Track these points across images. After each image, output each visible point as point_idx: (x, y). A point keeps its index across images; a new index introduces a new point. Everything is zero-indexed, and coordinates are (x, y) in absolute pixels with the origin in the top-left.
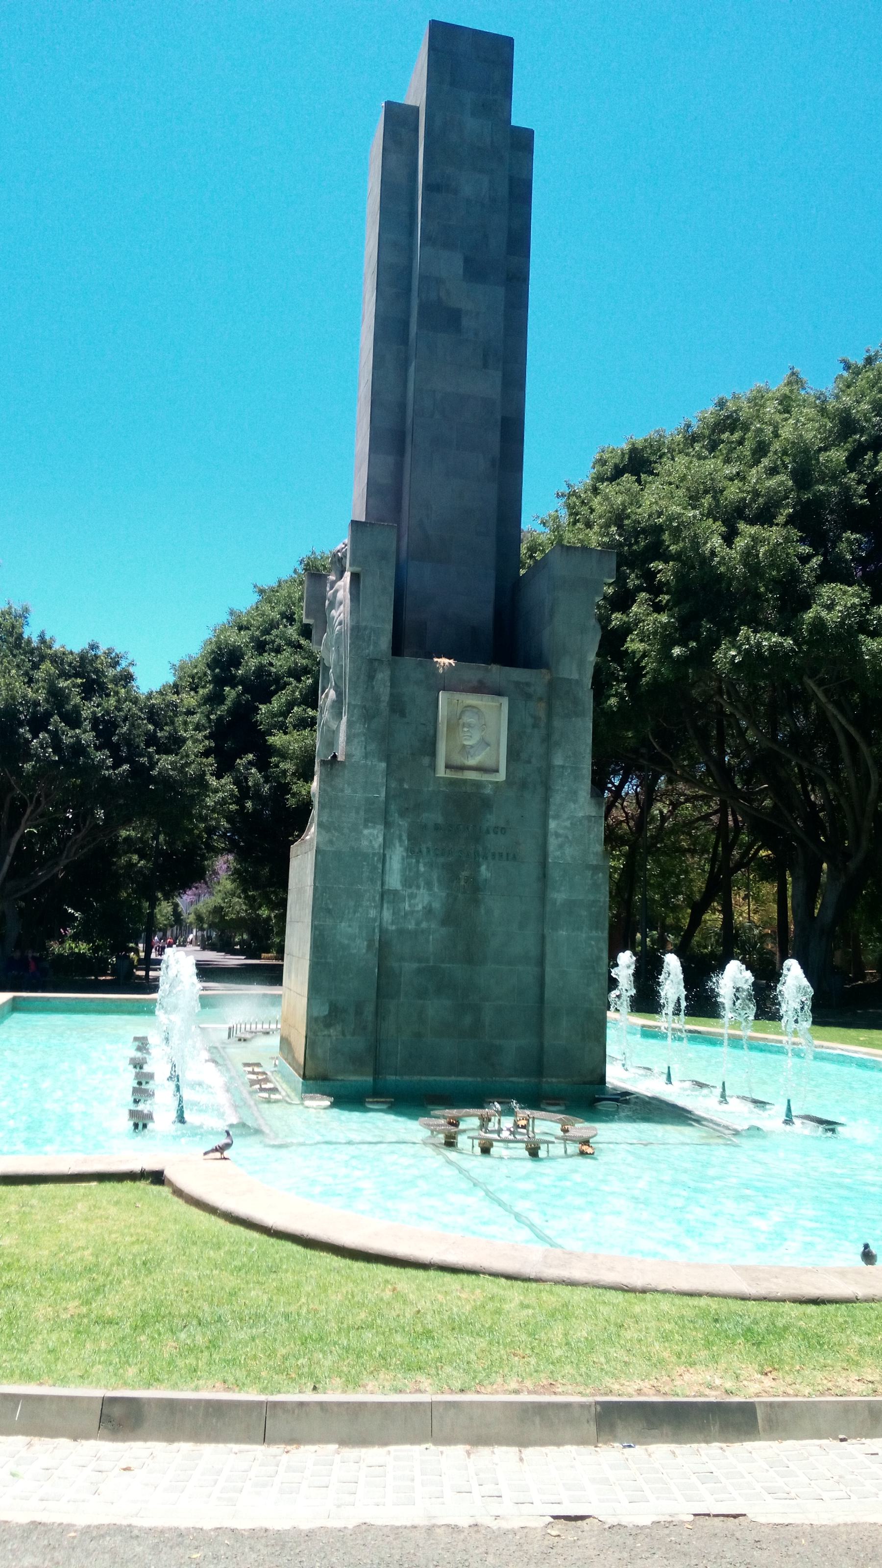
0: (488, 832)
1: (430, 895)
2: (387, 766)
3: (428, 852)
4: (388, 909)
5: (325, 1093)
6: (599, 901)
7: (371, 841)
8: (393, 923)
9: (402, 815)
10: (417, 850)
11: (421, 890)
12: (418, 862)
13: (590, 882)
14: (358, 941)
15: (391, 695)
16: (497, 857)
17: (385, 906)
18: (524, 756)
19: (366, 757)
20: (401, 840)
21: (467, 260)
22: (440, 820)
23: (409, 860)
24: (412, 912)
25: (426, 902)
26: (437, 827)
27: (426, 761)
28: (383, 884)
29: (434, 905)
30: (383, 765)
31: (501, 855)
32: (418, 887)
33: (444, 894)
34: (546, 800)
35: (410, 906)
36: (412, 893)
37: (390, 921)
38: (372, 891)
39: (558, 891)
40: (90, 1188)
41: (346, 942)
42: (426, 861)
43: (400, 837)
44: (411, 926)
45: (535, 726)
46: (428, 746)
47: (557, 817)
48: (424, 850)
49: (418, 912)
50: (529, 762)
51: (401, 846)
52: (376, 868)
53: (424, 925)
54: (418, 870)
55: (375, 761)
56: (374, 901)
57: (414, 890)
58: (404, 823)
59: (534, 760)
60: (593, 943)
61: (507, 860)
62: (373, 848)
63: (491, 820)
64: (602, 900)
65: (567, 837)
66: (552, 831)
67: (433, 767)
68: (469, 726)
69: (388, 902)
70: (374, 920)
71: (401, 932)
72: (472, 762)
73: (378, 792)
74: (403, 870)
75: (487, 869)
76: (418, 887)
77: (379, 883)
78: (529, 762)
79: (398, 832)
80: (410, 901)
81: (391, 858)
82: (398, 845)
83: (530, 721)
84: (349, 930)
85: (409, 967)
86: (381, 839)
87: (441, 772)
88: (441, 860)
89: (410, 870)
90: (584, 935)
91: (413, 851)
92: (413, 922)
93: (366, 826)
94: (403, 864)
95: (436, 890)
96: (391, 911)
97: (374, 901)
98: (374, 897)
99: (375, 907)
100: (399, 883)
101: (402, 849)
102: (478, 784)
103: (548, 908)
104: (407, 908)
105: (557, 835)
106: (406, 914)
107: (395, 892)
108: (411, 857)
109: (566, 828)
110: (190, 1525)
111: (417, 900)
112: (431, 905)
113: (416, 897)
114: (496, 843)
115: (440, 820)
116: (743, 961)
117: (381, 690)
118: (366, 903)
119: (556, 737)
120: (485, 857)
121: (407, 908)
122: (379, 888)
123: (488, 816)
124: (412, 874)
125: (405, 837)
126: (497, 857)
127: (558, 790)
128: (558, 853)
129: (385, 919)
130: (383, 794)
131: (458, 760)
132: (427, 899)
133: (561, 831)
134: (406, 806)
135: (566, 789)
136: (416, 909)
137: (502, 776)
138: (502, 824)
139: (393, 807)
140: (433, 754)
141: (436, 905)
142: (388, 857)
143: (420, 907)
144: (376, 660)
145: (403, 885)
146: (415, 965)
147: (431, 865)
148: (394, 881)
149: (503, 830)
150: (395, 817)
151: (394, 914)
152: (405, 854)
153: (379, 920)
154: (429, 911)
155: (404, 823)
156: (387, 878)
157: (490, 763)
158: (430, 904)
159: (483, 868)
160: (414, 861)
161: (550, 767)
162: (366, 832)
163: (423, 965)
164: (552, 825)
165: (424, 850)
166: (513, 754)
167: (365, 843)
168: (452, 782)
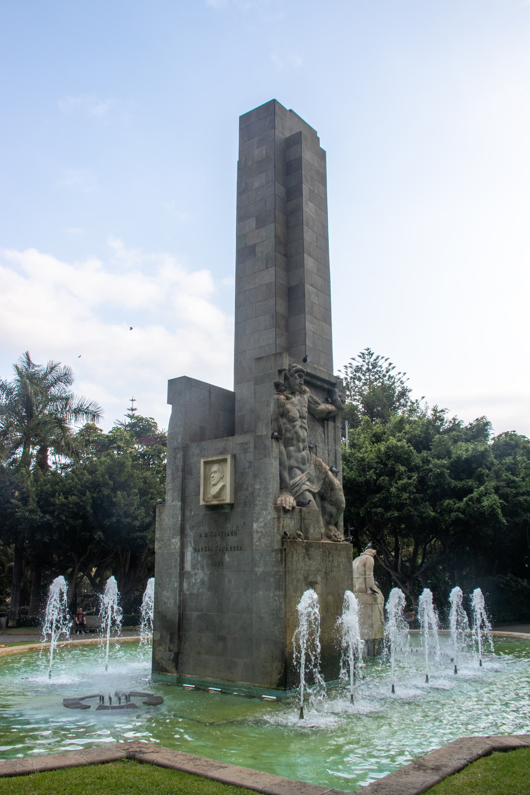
1: (203, 573)
3: (202, 549)
5: (49, 586)
6: (280, 571)
8: (188, 590)
12: (198, 555)
13: (274, 560)
14: (171, 600)
19: (173, 501)
20: (191, 544)
22: (207, 530)
24: (196, 583)
32: (198, 569)
33: (209, 572)
35: (195, 580)
39: (259, 567)
43: (191, 541)
44: (195, 592)
53: (201, 590)
56: (177, 578)
60: (277, 598)
62: (176, 549)
64: (281, 570)
65: (262, 533)
71: (191, 594)
74: (192, 559)
76: (198, 569)
78: (247, 489)
84: (167, 594)
85: (195, 614)
92: (196, 589)
93: (173, 538)
99: (177, 581)
104: (194, 581)
105: (257, 532)
106: (193, 584)
109: (261, 527)
115: (207, 530)
116: (320, 595)
121: (194, 581)
123: (228, 525)
125: (192, 542)
128: (258, 543)
132: (202, 575)
133: (259, 530)
135: (261, 503)
136: (197, 581)
138: (234, 529)
141: (206, 579)
145: (192, 568)
146: (197, 613)
154: (203, 582)
158: (203, 578)
159: (226, 556)
162: (173, 541)
163: (200, 613)
165: (200, 548)
167: (173, 547)
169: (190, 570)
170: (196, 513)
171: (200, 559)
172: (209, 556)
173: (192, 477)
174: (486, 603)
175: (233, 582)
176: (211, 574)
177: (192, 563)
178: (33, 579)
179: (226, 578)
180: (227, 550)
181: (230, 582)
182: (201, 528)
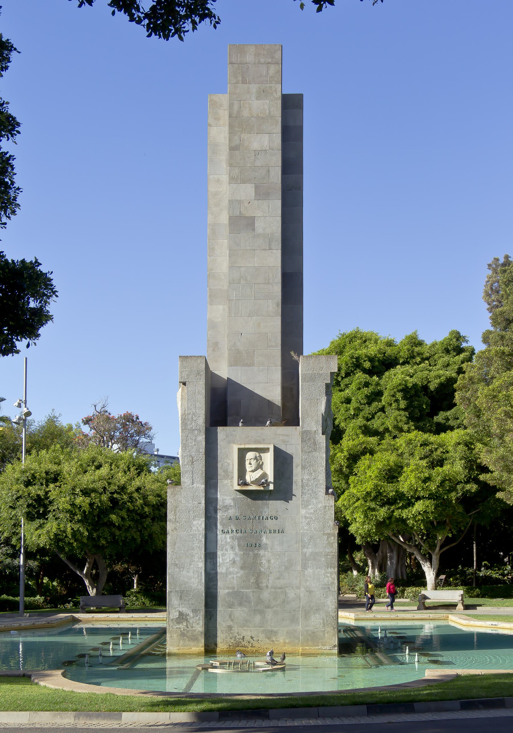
21: (257, 187)
25: (231, 558)
35: (222, 560)
40: (236, 359)
41: (186, 580)
56: (201, 559)
60: (329, 575)
75: (266, 538)
90: (323, 571)
97: (201, 559)
109: (311, 513)
110: (443, 339)
111: (226, 557)
118: (196, 559)
132: (232, 556)
146: (227, 591)
158: (234, 559)
162: (195, 523)
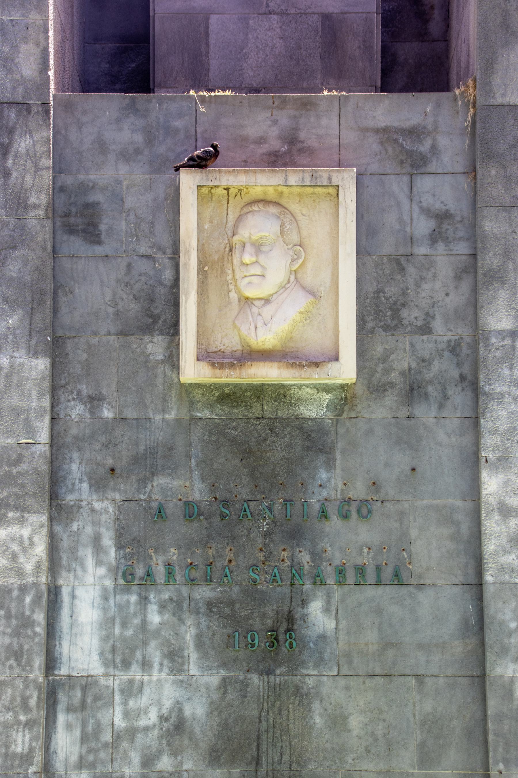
0: (324, 515)
2: (53, 366)
3: (170, 573)
4: (69, 727)
7: (14, 556)
9: (98, 485)
10: (140, 571)
11: (155, 675)
12: (144, 600)
15: (59, 189)
16: (351, 577)
17: (61, 718)
18: (411, 315)
22: (198, 492)
23: (122, 598)
24: (132, 733)
25: (167, 704)
26: (191, 511)
27: (155, 347)
28: (51, 663)
29: (188, 711)
30: (41, 365)
31: (360, 570)
33: (215, 681)
34: (474, 422)
35: (126, 715)
36: (131, 682)
37: (74, 758)
38: (19, 684)
42: (166, 596)
43: (96, 540)
45: (435, 237)
46: (158, 314)
47: (503, 462)
48: (160, 571)
49: (147, 729)
50: (426, 329)
51: (99, 563)
52: (27, 623)
54: (144, 622)
55: (21, 357)
56: (25, 707)
57: (135, 673)
58: (105, 507)
59: (438, 325)
61: (379, 583)
62: (20, 573)
63: (328, 482)
66: (491, 500)
67: (173, 360)
68: (258, 247)
69: (69, 709)
70: (27, 758)
72: (266, 338)
73: (30, 431)
74: (107, 623)
75: (326, 610)
76: (146, 665)
77: (39, 661)
78: (426, 329)
79: (89, 530)
80: (125, 703)
81: (73, 597)
82: (90, 562)
83: (423, 226)
86: (40, 549)
87: (192, 371)
88: (204, 593)
89: (124, 625)
91: (133, 576)
92: (135, 758)
94: (105, 610)
95: (193, 670)
96: (77, 733)
97: (25, 707)
98: (25, 701)
99: (29, 724)
100: (95, 657)
101: (102, 571)
102: (280, 393)
103: (493, 704)
104: (119, 722)
105: (505, 511)
106: (117, 737)
107: (88, 683)
108: (127, 590)
111: (144, 700)
112: (181, 711)
113: (140, 690)
114: (347, 540)
117: (28, 179)
119: (490, 259)
120: (318, 580)
122: (37, 674)
123: (323, 475)
124: (129, 633)
125: (108, 541)
126: (351, 577)
127: (502, 395)
129: (61, 755)
130: (44, 436)
131: (228, 341)
134: (110, 462)
136: (142, 723)
137: (346, 370)
138: (359, 490)
139: (75, 468)
140: (173, 329)
141: (196, 710)
142: (65, 592)
143: (153, 717)
144: (11, 103)
145: (106, 664)
147: (176, 607)
148: (82, 653)
149: (364, 510)
150: (80, 490)
151: (84, 738)
152: (109, 583)
153: (38, 758)
154: (176, 727)
155: (105, 507)
156: (65, 648)
157: (314, 340)
158: (178, 707)
159: (315, 608)
160: (134, 598)
161: (479, 334)
164: (491, 484)
165: (160, 571)
166: (378, 314)
168: (229, 397)
169: (96, 668)
170: (130, 414)
171: (155, 618)
172: (210, 605)
173: (99, 250)
174: (260, 361)
175: (355, 722)
176: (224, 684)
177: (105, 639)
178: (173, 715)
179: (316, 705)
180: (318, 580)
181: (338, 721)
182: (161, 481)
